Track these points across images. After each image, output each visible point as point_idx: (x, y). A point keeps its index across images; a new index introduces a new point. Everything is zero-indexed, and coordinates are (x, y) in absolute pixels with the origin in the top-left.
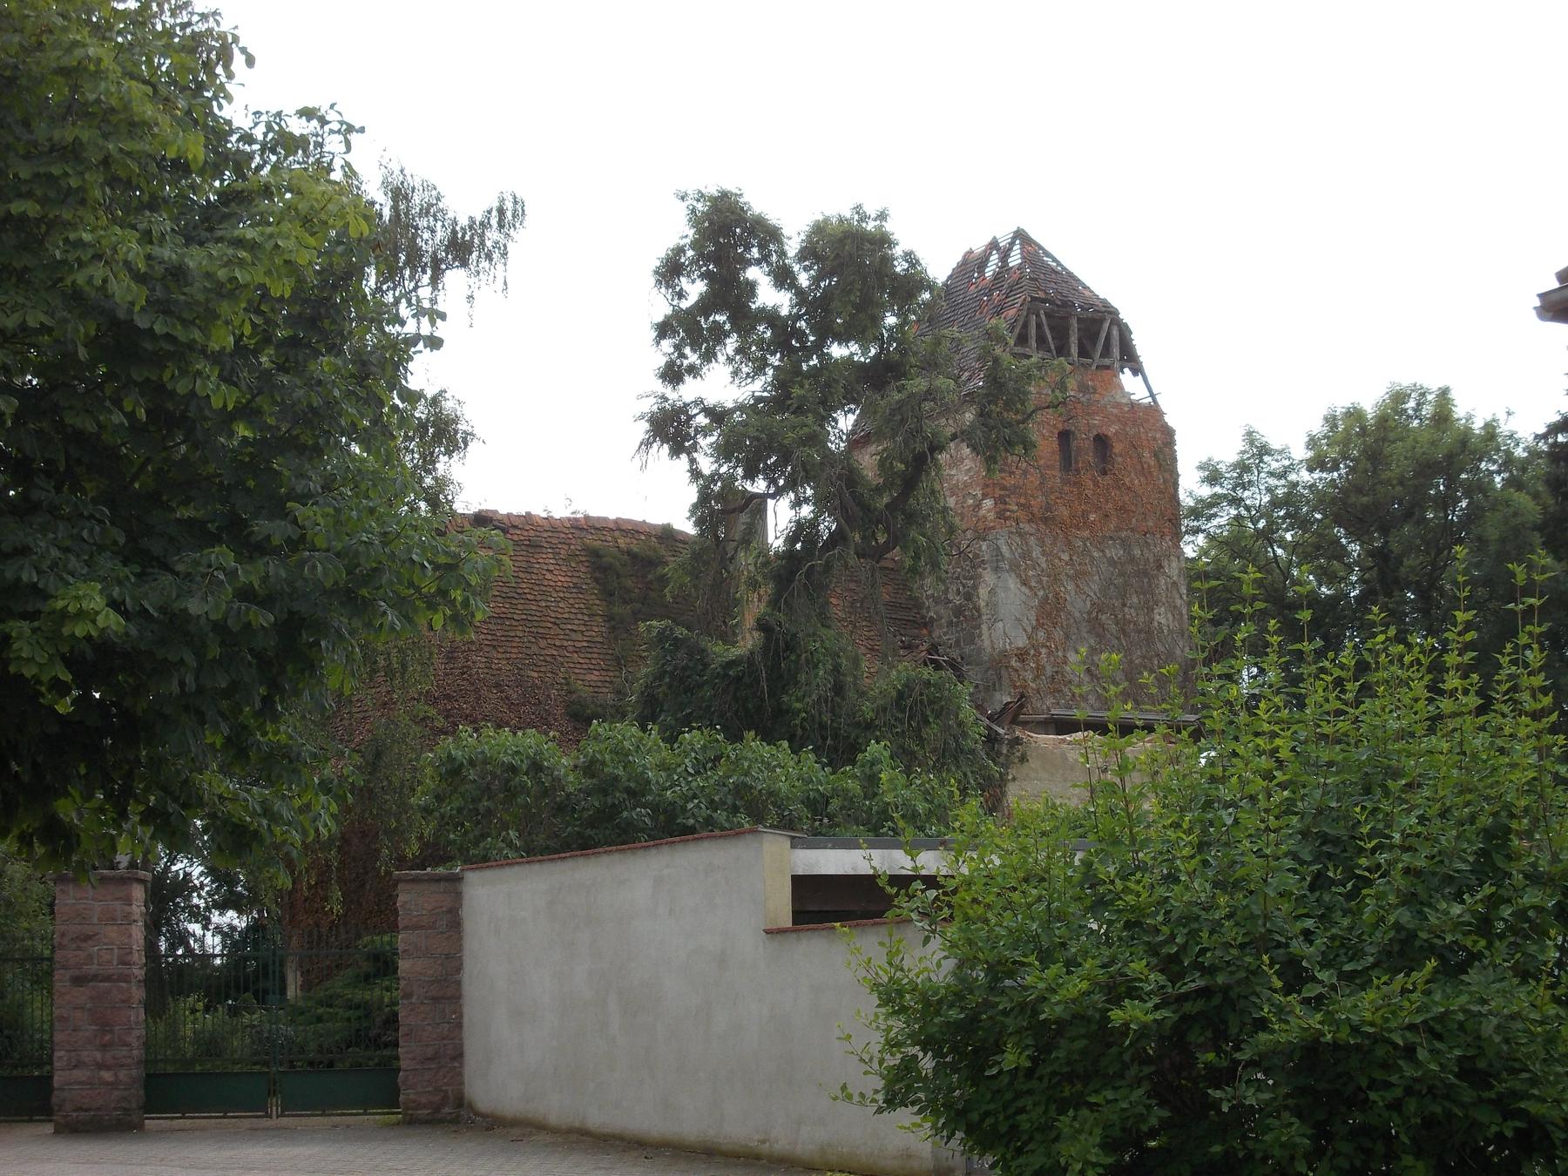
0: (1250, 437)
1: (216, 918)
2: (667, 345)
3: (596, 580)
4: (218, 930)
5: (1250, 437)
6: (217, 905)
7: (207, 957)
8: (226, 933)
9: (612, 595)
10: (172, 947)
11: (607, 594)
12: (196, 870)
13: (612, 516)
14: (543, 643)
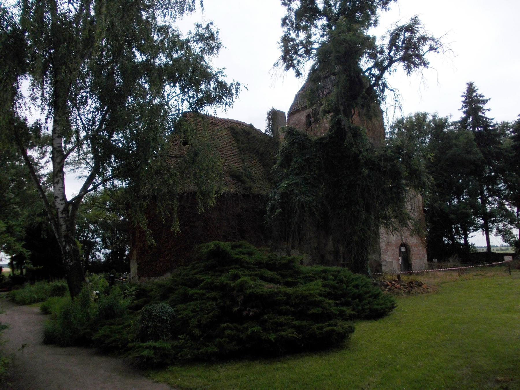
0: (467, 84)
1: (103, 251)
2: (285, 29)
3: (233, 136)
4: (103, 253)
5: (467, 84)
6: (103, 248)
7: (100, 260)
8: (105, 255)
9: (238, 141)
10: (92, 258)
11: (237, 141)
12: (98, 240)
13: (236, 120)
14: (220, 153)
